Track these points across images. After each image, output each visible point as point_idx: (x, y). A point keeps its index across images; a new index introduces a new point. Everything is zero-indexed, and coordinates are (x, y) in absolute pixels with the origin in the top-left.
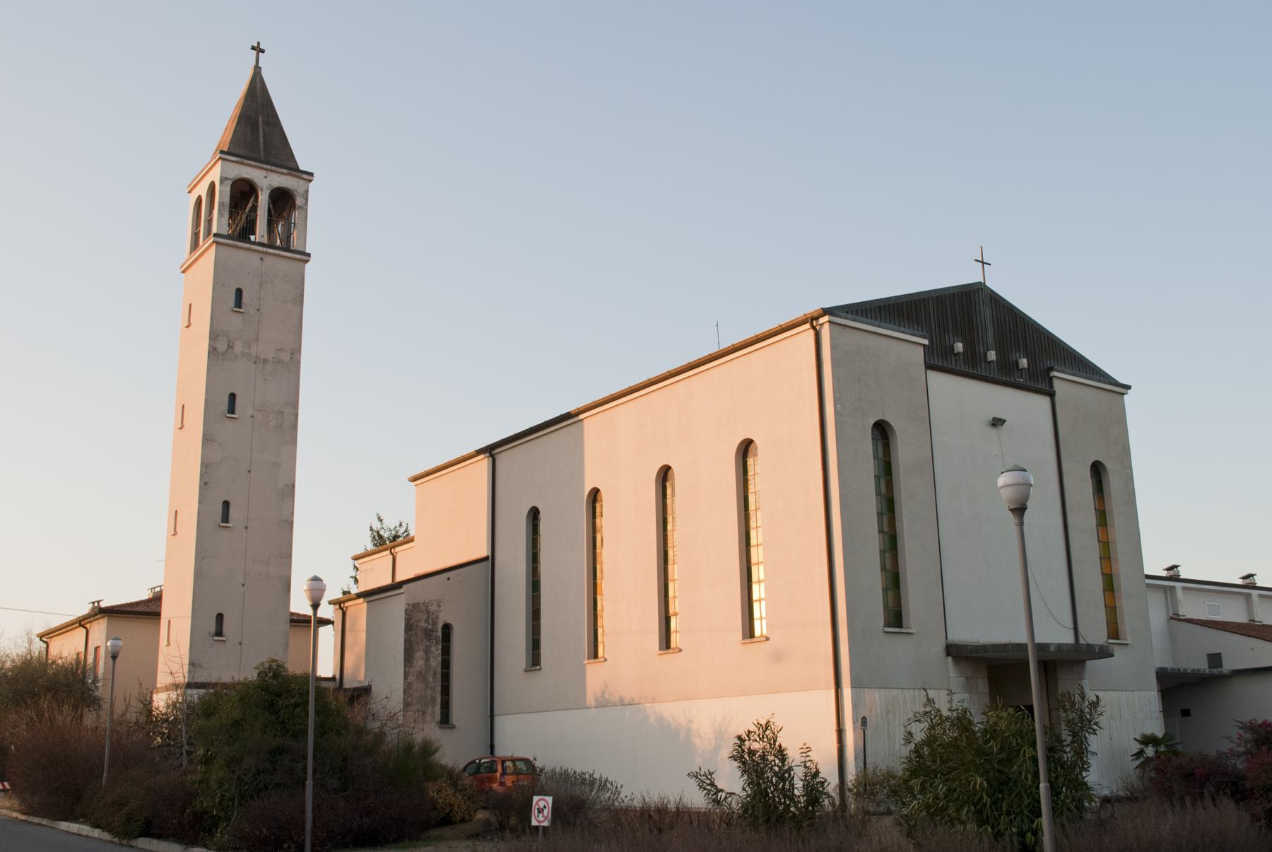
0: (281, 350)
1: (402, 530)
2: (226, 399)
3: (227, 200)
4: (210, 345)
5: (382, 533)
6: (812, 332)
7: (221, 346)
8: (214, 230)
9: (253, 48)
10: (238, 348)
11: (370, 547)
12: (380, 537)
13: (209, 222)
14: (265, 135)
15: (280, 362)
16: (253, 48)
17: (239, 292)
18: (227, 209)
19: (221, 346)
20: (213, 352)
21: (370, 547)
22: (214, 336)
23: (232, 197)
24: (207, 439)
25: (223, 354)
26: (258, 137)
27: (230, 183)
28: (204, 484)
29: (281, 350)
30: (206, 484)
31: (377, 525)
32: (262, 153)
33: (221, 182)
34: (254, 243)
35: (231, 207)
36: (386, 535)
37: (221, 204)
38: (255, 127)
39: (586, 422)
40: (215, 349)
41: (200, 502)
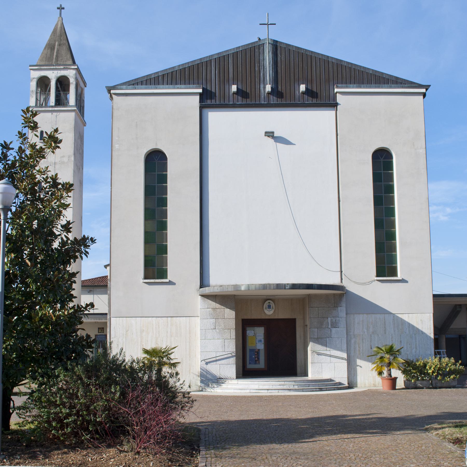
0: (63, 157)
14: (58, 50)
15: (63, 163)
26: (53, 53)
29: (63, 157)
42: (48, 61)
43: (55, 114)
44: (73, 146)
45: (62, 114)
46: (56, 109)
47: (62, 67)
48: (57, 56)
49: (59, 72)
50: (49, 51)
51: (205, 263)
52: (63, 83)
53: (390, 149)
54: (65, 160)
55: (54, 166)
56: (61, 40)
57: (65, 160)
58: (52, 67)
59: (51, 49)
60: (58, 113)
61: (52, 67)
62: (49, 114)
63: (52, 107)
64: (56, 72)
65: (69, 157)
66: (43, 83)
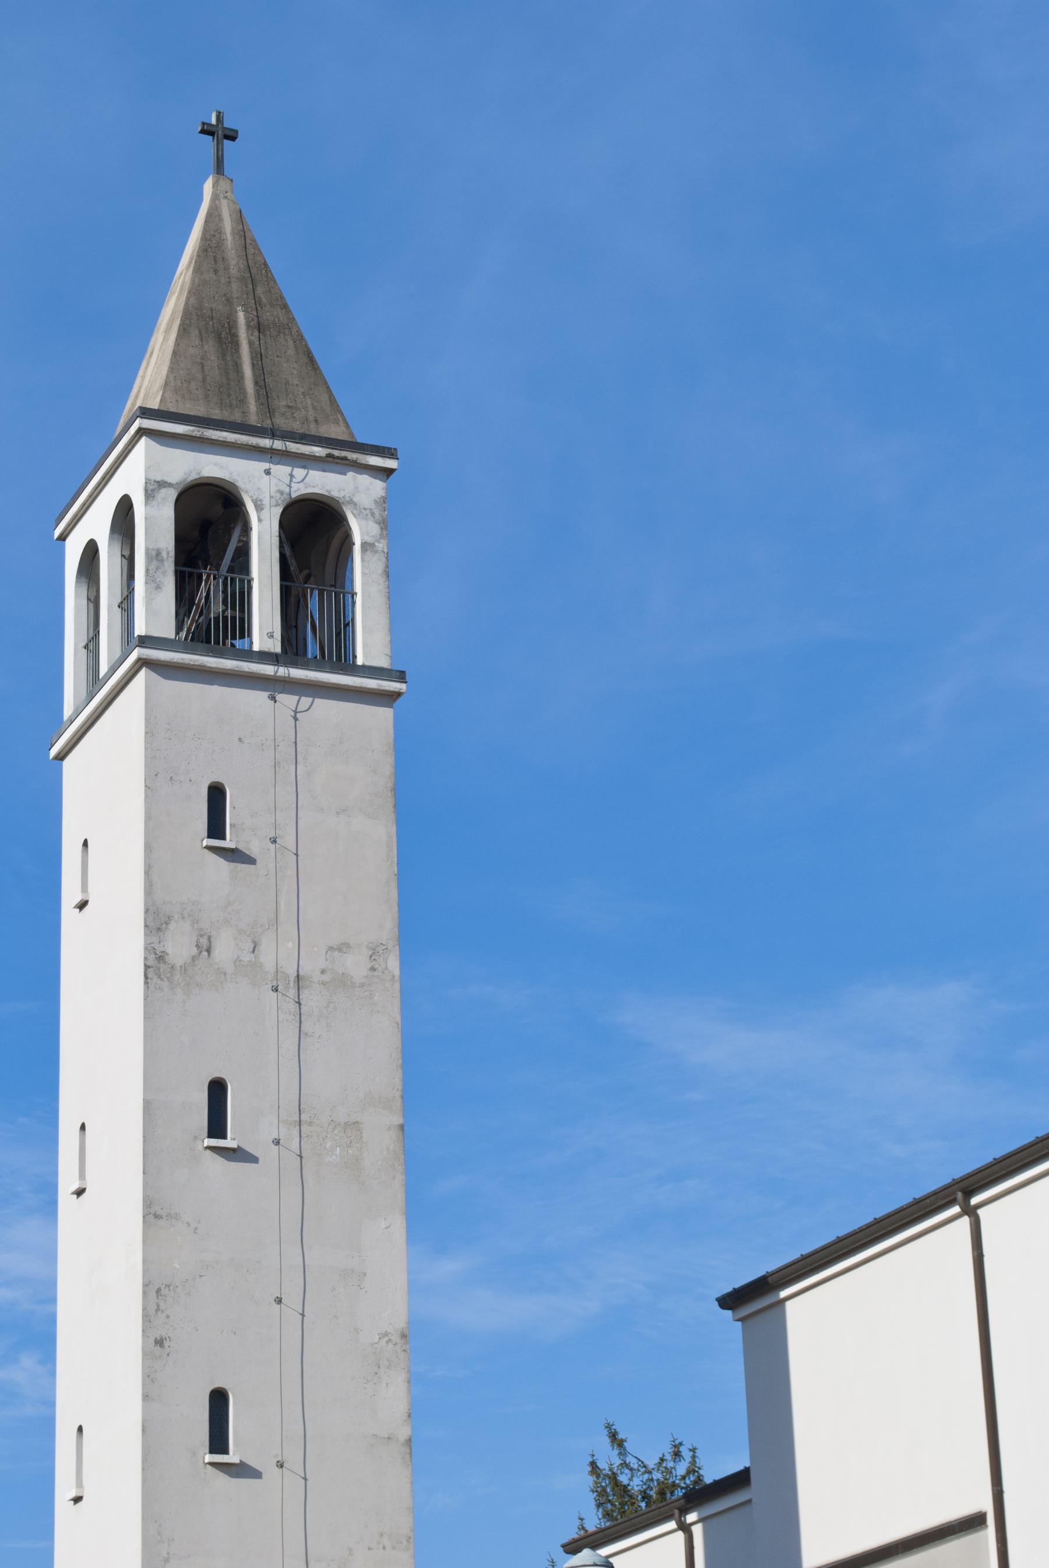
0: (343, 948)
1: (681, 1469)
2: (201, 1098)
3: (167, 542)
4: (149, 949)
5: (624, 1479)
6: (965, 1220)
7: (179, 947)
8: (140, 629)
9: (207, 131)
10: (224, 950)
11: (594, 1521)
12: (623, 1490)
13: (126, 604)
14: (258, 358)
15: (343, 982)
16: (207, 131)
17: (216, 795)
18: (169, 567)
19: (179, 947)
20: (156, 964)
21: (594, 1521)
22: (156, 922)
23: (180, 540)
24: (154, 1213)
25: (184, 969)
26: (238, 367)
27: (172, 495)
28: (156, 1345)
29: (343, 948)
30: (160, 1342)
31: (608, 1458)
32: (252, 406)
33: (149, 495)
34: (249, 655)
35: (177, 563)
36: (636, 1485)
37: (154, 556)
38: (227, 340)
39: (789, 1304)
40: (161, 958)
41: (146, 1397)
42: (221, 405)
43: (288, 700)
44: (394, 893)
45: (324, 708)
46: (282, 671)
47: (318, 451)
48: (260, 383)
49: (300, 473)
50: (211, 347)
51: (89, 722)
52: (314, 533)
53: (240, 484)
54: (355, 965)
55: (292, 992)
56: (258, 302)
57: (355, 965)
58: (266, 443)
59: (219, 339)
60: (306, 701)
61: (266, 443)
62: (259, 698)
63: (264, 657)
64: (281, 471)
65: (375, 952)
66: (207, 523)
